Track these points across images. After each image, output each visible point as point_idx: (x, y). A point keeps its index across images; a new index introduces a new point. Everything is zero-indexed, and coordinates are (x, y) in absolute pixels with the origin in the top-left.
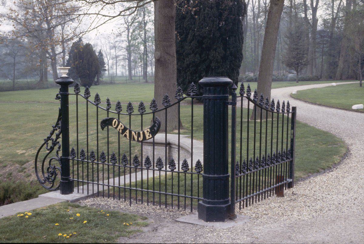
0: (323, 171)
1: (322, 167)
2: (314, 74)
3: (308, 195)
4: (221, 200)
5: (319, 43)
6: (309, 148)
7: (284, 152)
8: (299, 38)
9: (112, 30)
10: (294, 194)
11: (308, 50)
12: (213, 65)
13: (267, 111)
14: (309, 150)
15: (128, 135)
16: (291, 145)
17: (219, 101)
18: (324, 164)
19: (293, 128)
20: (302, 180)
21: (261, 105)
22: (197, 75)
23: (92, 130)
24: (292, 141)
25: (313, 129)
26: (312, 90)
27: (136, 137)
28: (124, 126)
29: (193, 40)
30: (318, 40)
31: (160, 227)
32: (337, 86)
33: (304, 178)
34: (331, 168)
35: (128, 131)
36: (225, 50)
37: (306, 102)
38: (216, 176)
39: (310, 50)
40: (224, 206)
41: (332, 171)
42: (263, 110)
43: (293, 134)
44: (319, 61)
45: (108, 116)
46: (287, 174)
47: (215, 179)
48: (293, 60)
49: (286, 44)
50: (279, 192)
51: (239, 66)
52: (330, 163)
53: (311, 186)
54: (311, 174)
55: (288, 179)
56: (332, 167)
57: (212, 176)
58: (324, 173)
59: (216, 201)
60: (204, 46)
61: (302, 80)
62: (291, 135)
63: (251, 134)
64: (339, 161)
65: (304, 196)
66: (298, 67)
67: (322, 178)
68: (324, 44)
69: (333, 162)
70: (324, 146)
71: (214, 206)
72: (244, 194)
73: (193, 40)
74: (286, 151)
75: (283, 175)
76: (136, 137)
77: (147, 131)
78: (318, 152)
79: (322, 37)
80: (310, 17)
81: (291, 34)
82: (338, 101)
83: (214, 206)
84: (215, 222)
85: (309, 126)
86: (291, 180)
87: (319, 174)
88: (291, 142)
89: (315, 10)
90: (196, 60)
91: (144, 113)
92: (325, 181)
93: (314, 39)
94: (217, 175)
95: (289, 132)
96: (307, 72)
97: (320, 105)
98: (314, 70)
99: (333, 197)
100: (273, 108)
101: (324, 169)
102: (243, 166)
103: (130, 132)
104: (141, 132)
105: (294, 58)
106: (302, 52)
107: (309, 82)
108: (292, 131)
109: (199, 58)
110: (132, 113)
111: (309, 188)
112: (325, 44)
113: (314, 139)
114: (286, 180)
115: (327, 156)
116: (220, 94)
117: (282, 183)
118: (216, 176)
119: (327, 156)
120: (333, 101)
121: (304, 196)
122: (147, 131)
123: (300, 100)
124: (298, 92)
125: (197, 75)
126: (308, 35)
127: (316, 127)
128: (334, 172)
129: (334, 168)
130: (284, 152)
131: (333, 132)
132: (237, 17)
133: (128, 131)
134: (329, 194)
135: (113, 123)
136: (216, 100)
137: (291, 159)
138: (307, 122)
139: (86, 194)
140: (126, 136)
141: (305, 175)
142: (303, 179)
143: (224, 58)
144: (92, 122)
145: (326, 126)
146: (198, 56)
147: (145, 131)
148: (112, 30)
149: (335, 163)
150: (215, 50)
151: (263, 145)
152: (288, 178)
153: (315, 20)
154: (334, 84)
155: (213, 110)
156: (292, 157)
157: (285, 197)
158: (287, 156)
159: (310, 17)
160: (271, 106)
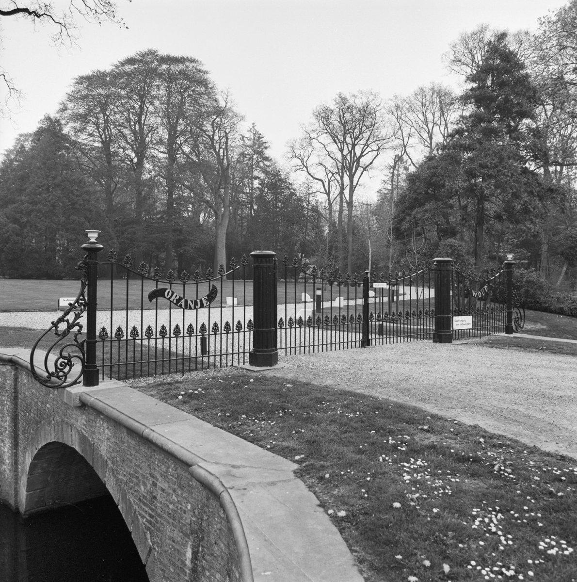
9: (127, 28)
35: (183, 301)
147: (203, 299)
148: (127, 28)
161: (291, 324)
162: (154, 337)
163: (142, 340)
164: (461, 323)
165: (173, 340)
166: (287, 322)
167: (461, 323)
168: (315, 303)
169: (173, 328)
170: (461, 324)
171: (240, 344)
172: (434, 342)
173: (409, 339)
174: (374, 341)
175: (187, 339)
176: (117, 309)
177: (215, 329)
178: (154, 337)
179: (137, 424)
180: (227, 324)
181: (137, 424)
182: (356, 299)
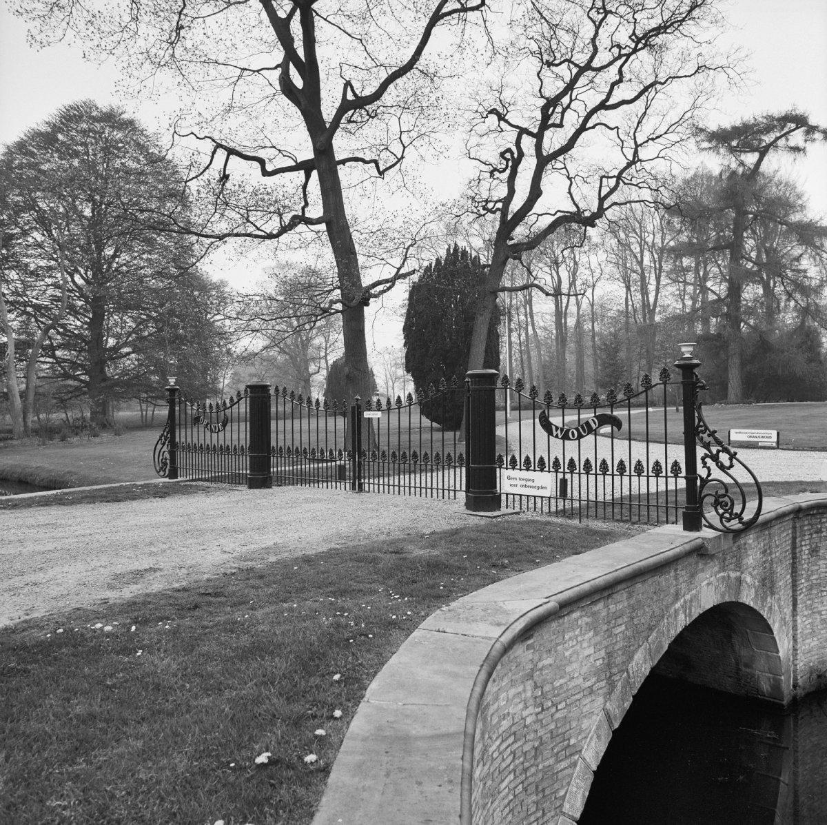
8: (616, 350)
161: (657, 470)
162: (610, 472)
163: (564, 473)
164: (523, 483)
165: (635, 480)
166: (537, 462)
167: (523, 483)
168: (248, 423)
169: (616, 463)
170: (522, 486)
171: (615, 485)
172: (250, 487)
173: (325, 484)
174: (367, 485)
175: (584, 477)
176: (651, 442)
177: (557, 466)
178: (645, 474)
179: (662, 555)
180: (587, 461)
181: (662, 555)
182: (666, 443)
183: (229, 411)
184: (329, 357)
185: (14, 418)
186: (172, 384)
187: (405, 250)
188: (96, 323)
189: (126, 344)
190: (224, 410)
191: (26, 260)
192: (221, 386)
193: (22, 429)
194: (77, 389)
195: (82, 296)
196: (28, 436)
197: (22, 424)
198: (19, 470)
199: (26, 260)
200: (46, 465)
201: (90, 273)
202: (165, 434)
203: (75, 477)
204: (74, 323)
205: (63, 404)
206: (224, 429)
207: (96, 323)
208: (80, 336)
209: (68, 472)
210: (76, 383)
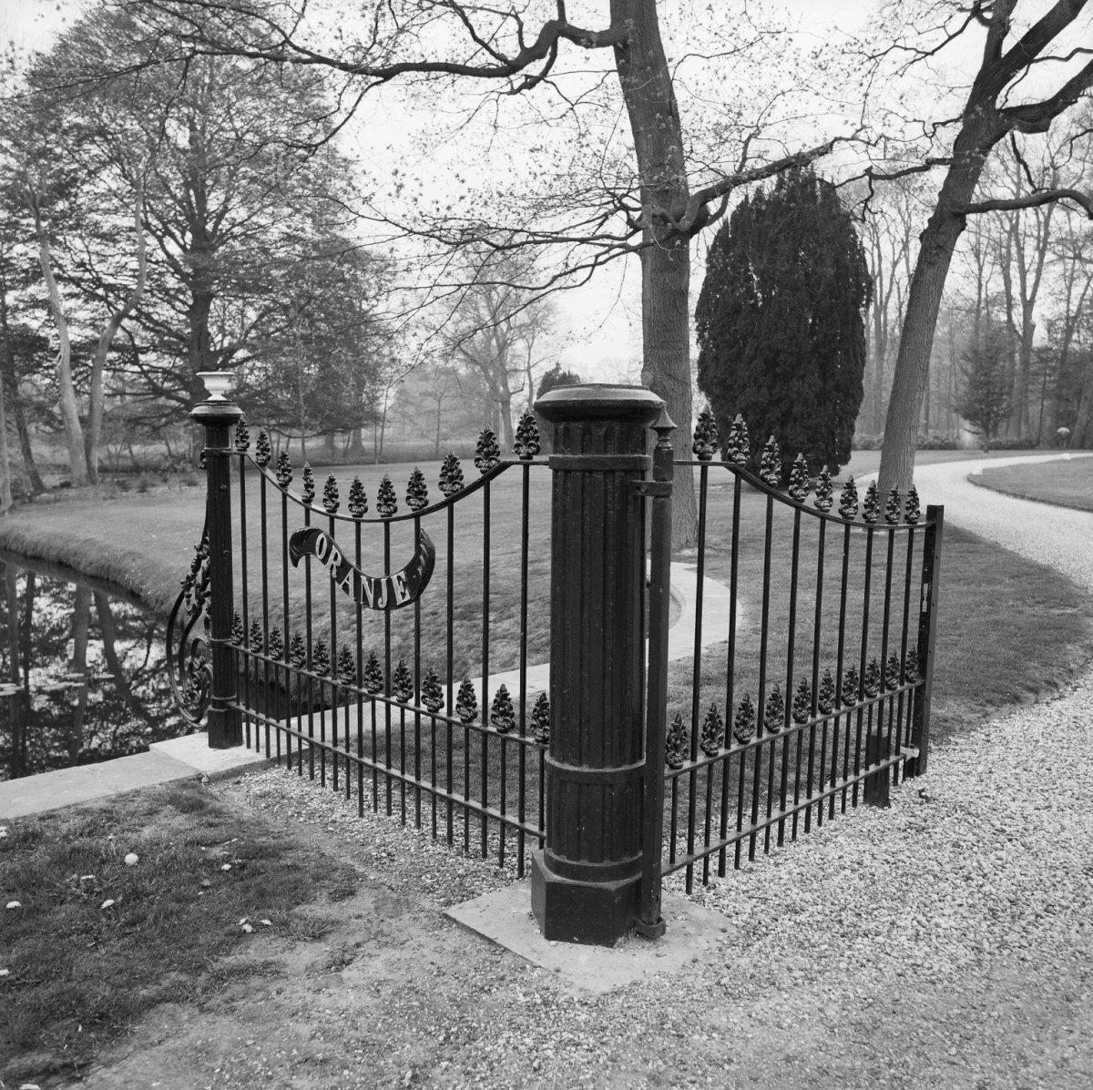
0: (1032, 696)
1: (1031, 684)
2: (1023, 437)
3: (972, 810)
4: (607, 863)
5: (1036, 374)
6: (995, 617)
7: (893, 660)
8: (993, 360)
10: (926, 797)
11: (1011, 386)
12: (797, 410)
13: (823, 519)
14: (996, 623)
15: (351, 586)
16: (920, 634)
17: (600, 476)
18: (1035, 671)
19: (928, 576)
20: (962, 729)
21: (796, 497)
22: (763, 432)
23: (275, 568)
24: (925, 619)
25: (1013, 558)
26: (1016, 469)
27: (371, 596)
28: (343, 558)
29: (754, 357)
30: (1033, 369)
31: (370, 947)
32: (1073, 460)
33: (970, 723)
34: (1056, 685)
35: (351, 574)
36: (825, 381)
37: (1000, 492)
38: (586, 769)
39: (1016, 386)
40: (611, 885)
41: (1061, 697)
42: (803, 514)
43: (930, 598)
44: (1034, 410)
45: (307, 523)
46: (904, 720)
47: (581, 781)
48: (977, 406)
49: (965, 372)
50: (877, 793)
51: (855, 414)
52: (1055, 671)
53: (990, 758)
54: (993, 709)
55: (903, 749)
56: (1062, 683)
57: (572, 768)
58: (1036, 702)
59: (584, 863)
60: (778, 370)
61: (997, 448)
62: (922, 599)
63: (857, 568)
64: (1081, 662)
65: (960, 814)
66: (988, 420)
67: (1027, 724)
68: (1045, 374)
69: (1064, 664)
70: (1039, 609)
71: (577, 882)
72: (799, 743)
73: (754, 357)
74: (899, 658)
75: (885, 734)
76: (371, 596)
77: (399, 578)
78: (1019, 629)
79: (1042, 360)
80: (1018, 318)
81: (975, 352)
82: (1076, 493)
83: (577, 882)
84: (579, 946)
85: (1003, 551)
86: (916, 753)
87: (1018, 706)
88: (922, 623)
89: (1028, 305)
90: (761, 399)
91: (394, 516)
92: (1037, 741)
93: (1026, 363)
94: (590, 767)
95: (915, 587)
96: (1006, 433)
97: (1033, 499)
98: (1024, 428)
99: (1063, 828)
100: (851, 510)
101: (1035, 691)
102: (705, 729)
103: (357, 576)
104: (384, 581)
105: (980, 401)
106: (997, 390)
107: (1013, 452)
108: (926, 586)
109: (767, 396)
110: (365, 517)
111: (980, 768)
112: (1050, 375)
113: (1013, 586)
114: (897, 753)
115: (1047, 643)
116: (606, 452)
117: (883, 763)
118: (586, 769)
119: (1047, 643)
120: (1064, 491)
121: (960, 814)
122: (399, 578)
123: (988, 487)
124: (984, 470)
125: (763, 432)
126: (1011, 355)
127: (1022, 554)
128: (1065, 702)
129: (1067, 684)
130: (893, 660)
131: (1063, 567)
132: (852, 309)
133: (351, 574)
134: (1049, 807)
135: (318, 543)
136: (590, 472)
137: (919, 682)
138: (999, 539)
139: (261, 757)
140: (346, 588)
141: (972, 710)
142: (967, 727)
143: (822, 397)
144: (275, 537)
145: (1047, 551)
146: (764, 390)
147: (394, 578)
149: (1071, 671)
150: (803, 377)
151: (877, 597)
152: (906, 746)
153: (1029, 327)
154: (1067, 456)
155: (579, 512)
156: (923, 672)
157: (894, 809)
158: (902, 672)
159: (1018, 318)
160: (866, 506)
183: (434, 525)
184: (532, 370)
185: (73, 454)
186: (216, 397)
187: (742, 145)
188: (198, 312)
189: (242, 344)
190: (416, 516)
191: (95, 217)
192: (381, 408)
193: (84, 471)
194: (175, 410)
195: (178, 270)
196: (93, 483)
197: (84, 464)
198: (59, 543)
199: (95, 217)
200: (100, 538)
201: (189, 236)
202: (199, 579)
203: (139, 562)
204: (164, 312)
205: (156, 434)
206: (416, 598)
207: (198, 312)
208: (178, 335)
209: (131, 553)
210: (174, 403)
